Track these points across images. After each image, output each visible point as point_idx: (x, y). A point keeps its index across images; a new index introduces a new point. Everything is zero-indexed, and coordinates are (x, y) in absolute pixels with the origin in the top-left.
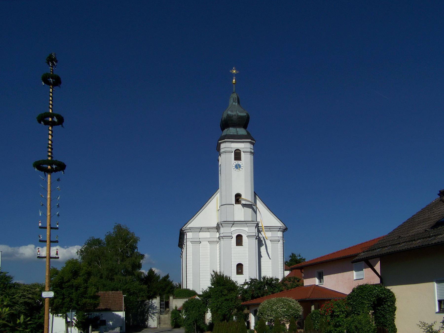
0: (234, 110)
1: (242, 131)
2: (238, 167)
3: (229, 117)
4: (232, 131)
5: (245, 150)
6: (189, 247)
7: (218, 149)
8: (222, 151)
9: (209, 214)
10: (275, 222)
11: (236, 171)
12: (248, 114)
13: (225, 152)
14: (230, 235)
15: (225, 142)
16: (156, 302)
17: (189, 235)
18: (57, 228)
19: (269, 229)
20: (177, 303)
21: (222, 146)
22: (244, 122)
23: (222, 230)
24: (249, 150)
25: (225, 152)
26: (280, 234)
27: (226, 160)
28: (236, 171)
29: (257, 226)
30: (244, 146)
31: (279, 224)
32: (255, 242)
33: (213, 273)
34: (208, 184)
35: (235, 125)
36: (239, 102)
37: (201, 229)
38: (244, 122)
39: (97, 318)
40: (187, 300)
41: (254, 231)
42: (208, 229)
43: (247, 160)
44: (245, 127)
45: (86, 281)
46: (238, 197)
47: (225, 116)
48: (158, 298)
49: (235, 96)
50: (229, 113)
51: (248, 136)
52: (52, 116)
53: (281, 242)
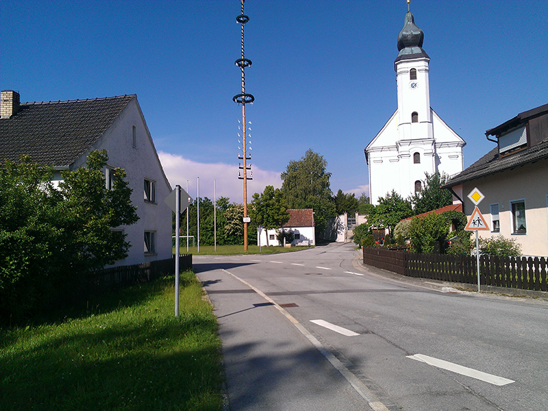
0: (410, 30)
1: (416, 50)
2: (414, 86)
3: (404, 37)
4: (407, 51)
5: (420, 68)
6: (373, 166)
7: (396, 69)
8: (398, 71)
9: (390, 134)
10: (453, 137)
11: (413, 89)
12: (422, 32)
13: (401, 73)
14: (408, 153)
15: (401, 62)
16: (343, 219)
17: (372, 155)
18: (250, 158)
19: (447, 144)
20: (361, 220)
21: (399, 66)
22: (418, 41)
23: (401, 149)
24: (424, 68)
25: (401, 73)
26: (459, 149)
27: (403, 80)
28: (413, 89)
29: (434, 143)
30: (420, 65)
31: (458, 139)
32: (431, 159)
33: (391, 194)
34: (389, 106)
35: (410, 45)
36: (413, 21)
37: (382, 149)
38: (418, 41)
39: (291, 233)
40: (119, 263)
41: (430, 148)
42: (389, 148)
43: (422, 78)
44: (420, 45)
45: (278, 201)
46: (415, 115)
47: (400, 36)
48: (346, 215)
49: (409, 15)
50: (404, 33)
51: (424, 54)
52: (244, 60)
53: (460, 157)
